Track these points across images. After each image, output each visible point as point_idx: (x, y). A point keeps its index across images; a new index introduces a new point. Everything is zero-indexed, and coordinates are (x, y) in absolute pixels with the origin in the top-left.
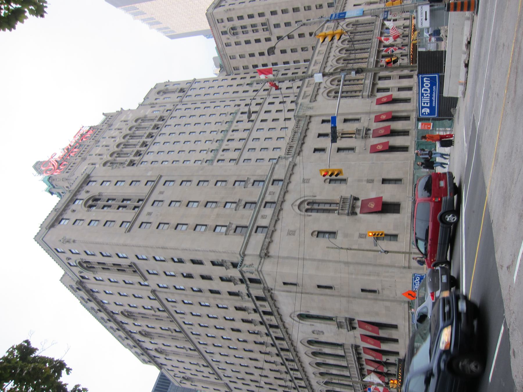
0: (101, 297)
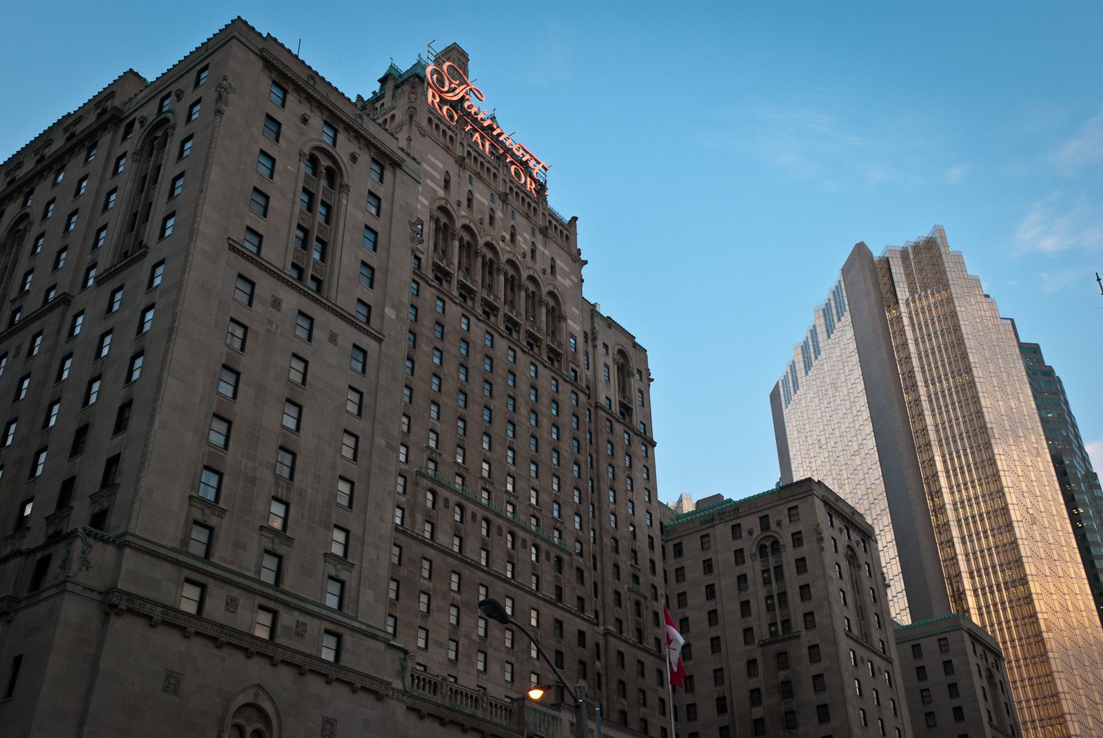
0: (75, 167)
